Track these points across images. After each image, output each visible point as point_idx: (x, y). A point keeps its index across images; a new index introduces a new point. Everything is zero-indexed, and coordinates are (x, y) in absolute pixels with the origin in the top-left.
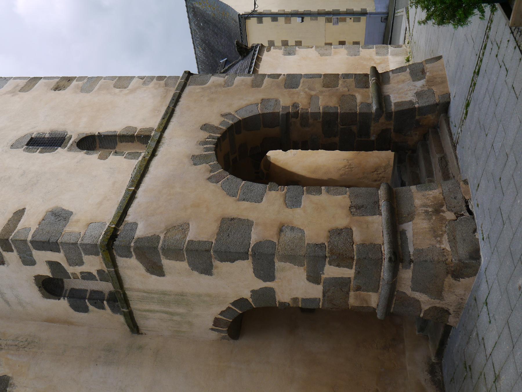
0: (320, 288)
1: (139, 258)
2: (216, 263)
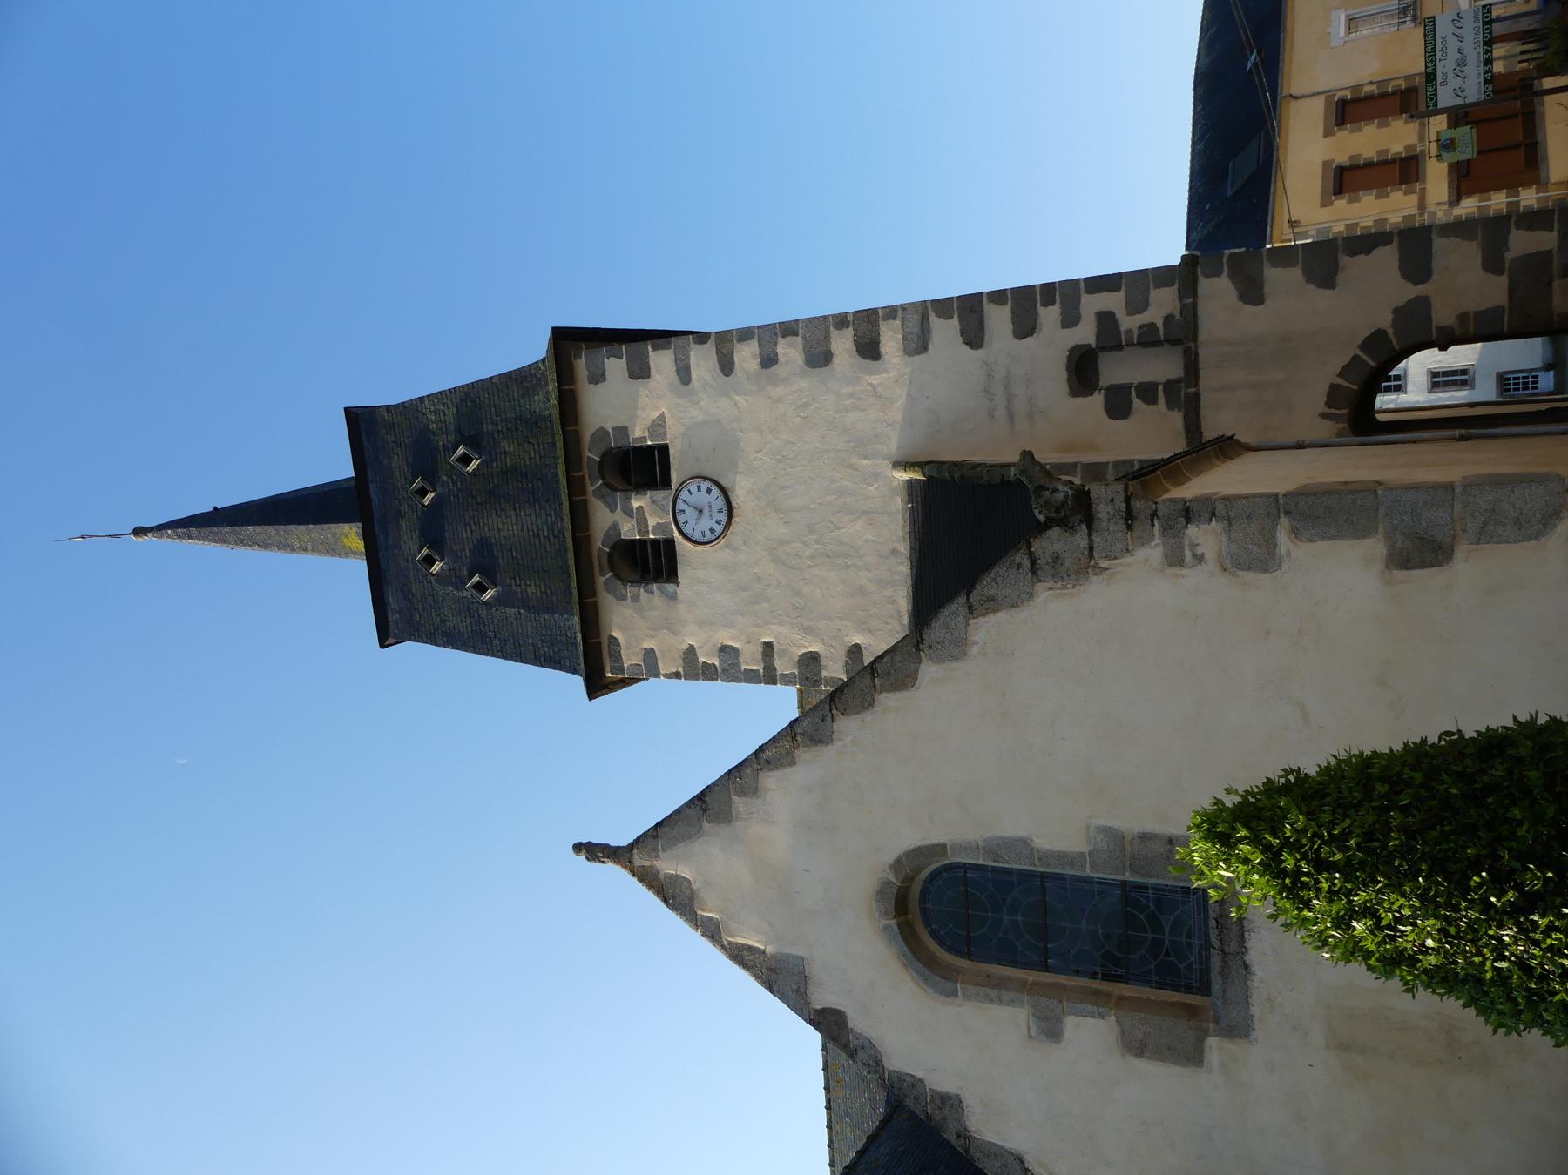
0: (1503, 281)
1: (1233, 276)
2: (1344, 260)
